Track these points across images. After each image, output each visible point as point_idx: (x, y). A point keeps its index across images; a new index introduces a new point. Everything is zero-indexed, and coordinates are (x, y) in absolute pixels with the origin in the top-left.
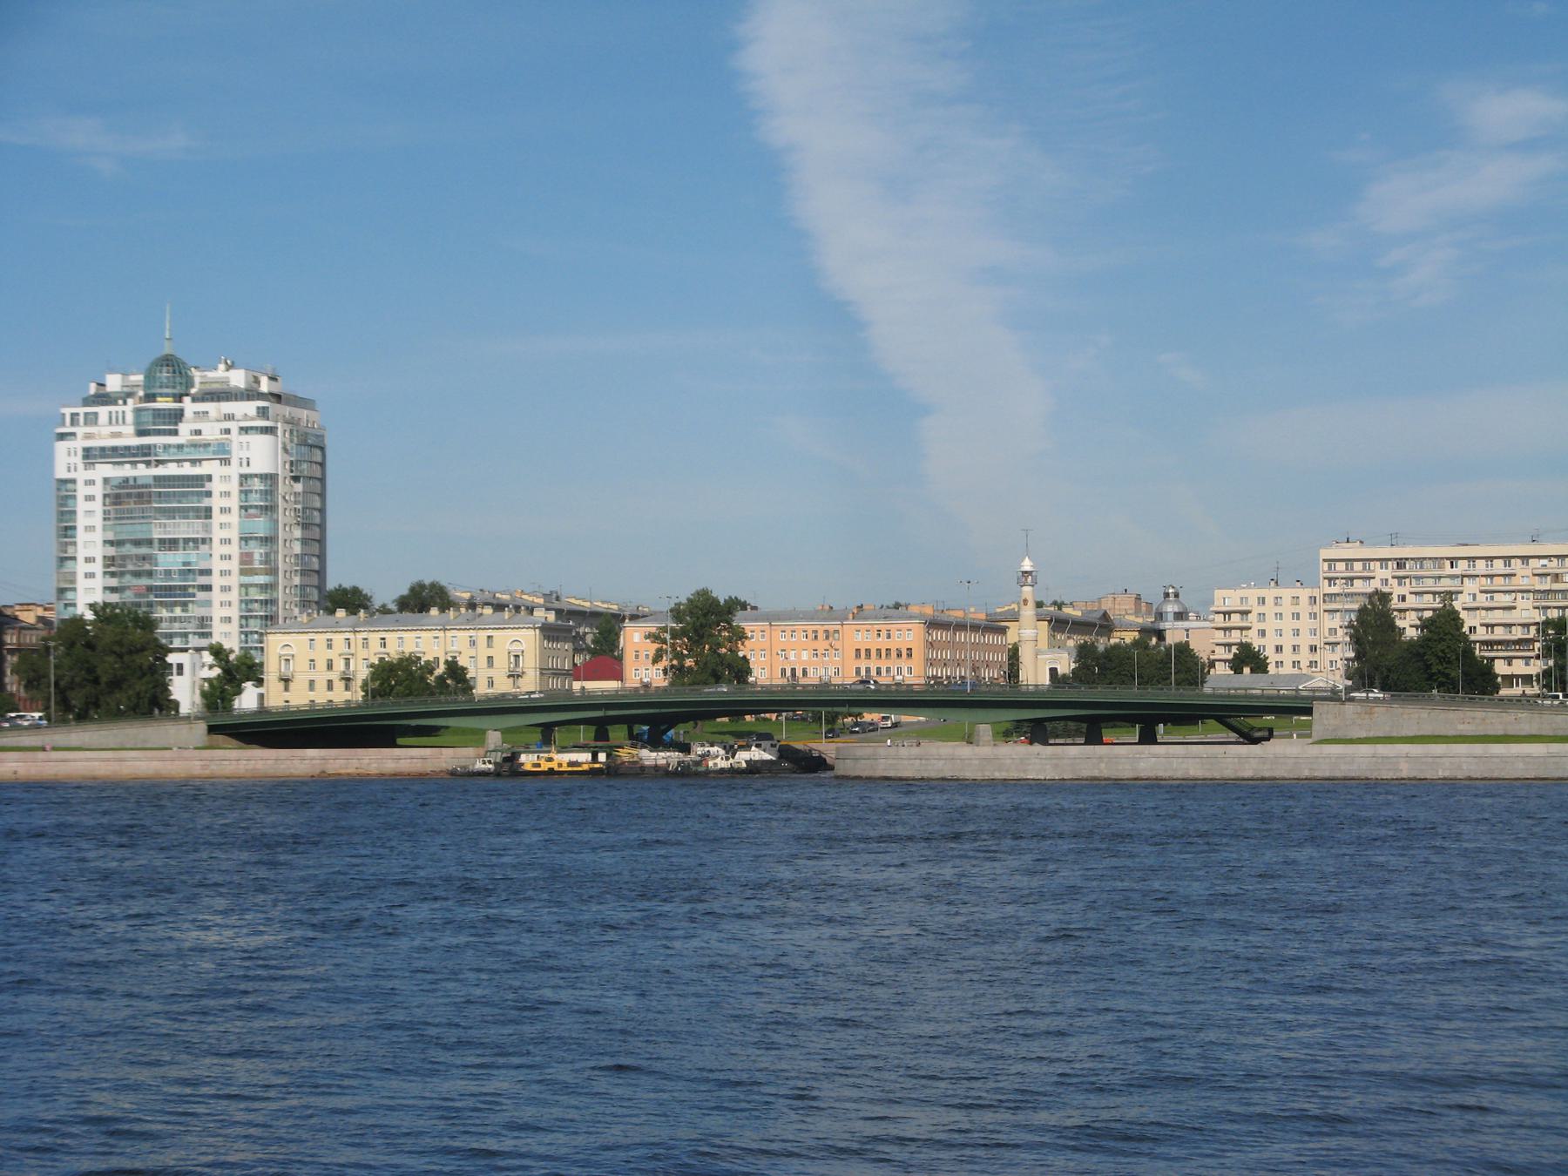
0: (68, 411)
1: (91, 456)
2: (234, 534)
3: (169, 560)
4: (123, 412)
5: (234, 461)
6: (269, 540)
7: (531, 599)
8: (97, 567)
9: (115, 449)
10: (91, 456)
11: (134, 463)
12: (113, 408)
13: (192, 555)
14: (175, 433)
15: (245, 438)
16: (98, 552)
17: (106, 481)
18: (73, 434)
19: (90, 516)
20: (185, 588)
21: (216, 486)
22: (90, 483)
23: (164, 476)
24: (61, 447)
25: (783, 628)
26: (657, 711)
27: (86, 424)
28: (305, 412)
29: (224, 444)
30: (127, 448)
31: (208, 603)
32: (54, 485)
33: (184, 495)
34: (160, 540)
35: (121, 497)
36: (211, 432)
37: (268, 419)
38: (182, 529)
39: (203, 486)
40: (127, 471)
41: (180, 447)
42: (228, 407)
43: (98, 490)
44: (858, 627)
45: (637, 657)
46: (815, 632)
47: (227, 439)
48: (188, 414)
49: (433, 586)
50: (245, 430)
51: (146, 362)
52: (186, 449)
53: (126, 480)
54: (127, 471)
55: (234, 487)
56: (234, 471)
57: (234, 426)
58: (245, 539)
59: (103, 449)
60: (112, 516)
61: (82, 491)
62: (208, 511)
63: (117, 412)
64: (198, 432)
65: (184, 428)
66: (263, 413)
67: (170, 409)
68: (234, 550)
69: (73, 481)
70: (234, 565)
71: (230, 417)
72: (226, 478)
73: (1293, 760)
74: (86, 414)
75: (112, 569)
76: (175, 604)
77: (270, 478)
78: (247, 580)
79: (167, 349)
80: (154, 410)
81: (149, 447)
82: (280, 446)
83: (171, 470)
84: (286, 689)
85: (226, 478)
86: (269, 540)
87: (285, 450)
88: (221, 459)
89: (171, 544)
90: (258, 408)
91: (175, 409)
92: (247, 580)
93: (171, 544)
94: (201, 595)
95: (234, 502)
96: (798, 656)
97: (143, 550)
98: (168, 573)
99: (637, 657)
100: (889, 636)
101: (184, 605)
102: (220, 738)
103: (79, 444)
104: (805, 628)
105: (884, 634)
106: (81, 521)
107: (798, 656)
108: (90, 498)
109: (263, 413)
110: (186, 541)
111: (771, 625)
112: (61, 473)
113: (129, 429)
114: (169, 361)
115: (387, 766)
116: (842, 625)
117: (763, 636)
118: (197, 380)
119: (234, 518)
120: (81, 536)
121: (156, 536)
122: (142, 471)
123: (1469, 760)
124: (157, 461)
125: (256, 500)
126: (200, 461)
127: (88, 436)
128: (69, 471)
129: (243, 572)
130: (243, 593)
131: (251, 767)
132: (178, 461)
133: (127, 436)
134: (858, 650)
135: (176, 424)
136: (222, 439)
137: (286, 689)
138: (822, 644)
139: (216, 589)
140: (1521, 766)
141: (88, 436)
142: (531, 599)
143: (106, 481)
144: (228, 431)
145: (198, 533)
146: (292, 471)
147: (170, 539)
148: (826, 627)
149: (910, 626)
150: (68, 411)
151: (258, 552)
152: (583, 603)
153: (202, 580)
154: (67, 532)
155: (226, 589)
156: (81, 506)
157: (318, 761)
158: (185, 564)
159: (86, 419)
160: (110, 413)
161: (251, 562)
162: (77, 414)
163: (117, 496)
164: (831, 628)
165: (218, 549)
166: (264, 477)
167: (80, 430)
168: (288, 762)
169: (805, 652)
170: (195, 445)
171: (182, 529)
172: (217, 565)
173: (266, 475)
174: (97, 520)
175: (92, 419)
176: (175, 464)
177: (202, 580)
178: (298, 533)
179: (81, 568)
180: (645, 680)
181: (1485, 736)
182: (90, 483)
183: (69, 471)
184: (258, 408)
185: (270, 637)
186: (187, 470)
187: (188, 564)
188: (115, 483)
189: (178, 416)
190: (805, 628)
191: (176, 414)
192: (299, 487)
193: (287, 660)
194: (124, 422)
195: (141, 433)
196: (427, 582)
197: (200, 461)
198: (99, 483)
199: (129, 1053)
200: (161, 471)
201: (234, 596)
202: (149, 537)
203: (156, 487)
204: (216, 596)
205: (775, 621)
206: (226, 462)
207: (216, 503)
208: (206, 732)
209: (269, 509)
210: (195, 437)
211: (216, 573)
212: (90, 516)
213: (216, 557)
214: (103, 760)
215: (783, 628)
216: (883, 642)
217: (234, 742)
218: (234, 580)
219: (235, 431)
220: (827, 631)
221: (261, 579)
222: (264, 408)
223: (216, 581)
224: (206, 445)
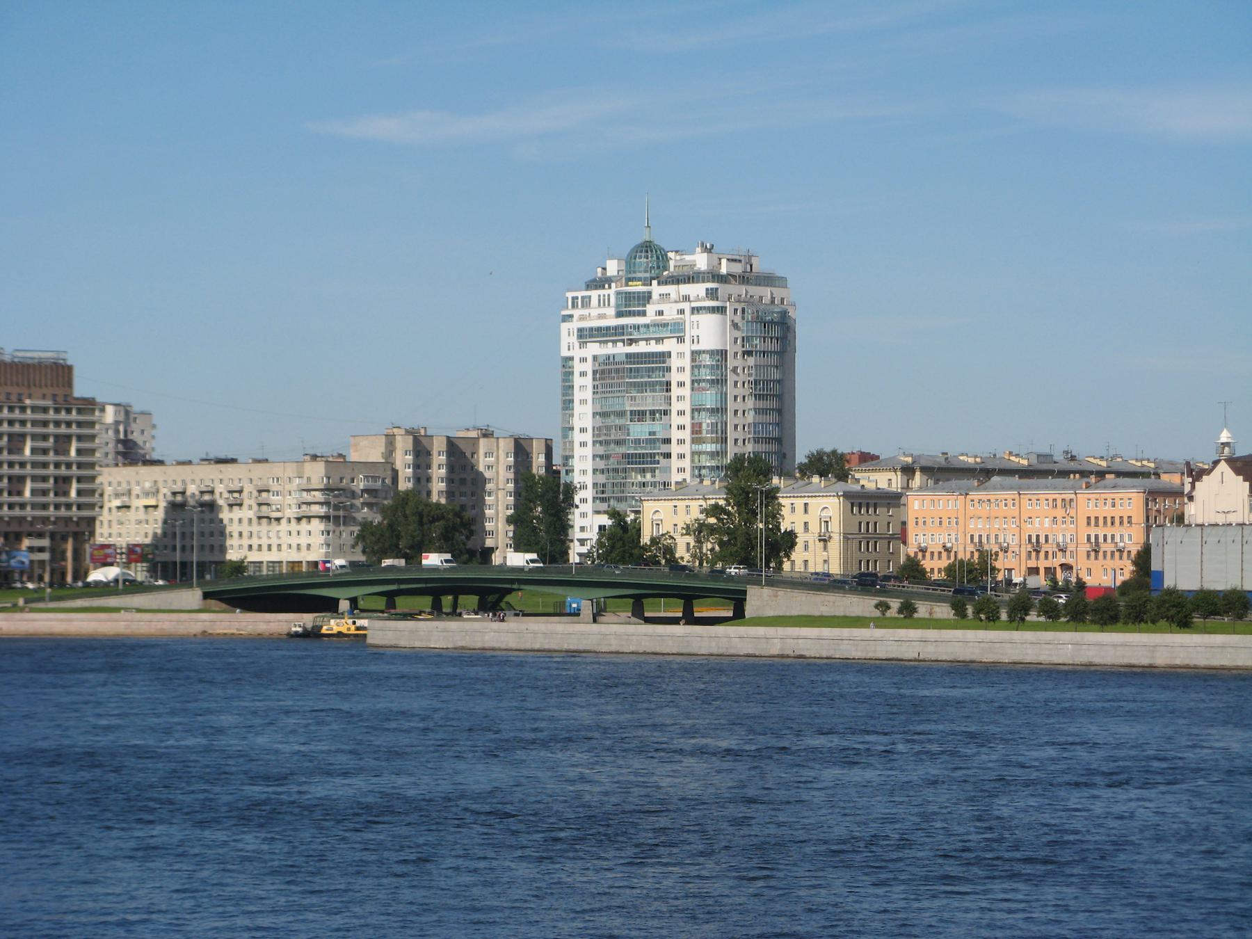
0: (570, 295)
1: (585, 335)
2: (686, 406)
3: (639, 430)
4: (609, 295)
5: (687, 339)
6: (720, 410)
7: (1017, 460)
8: (588, 437)
9: (599, 329)
10: (585, 335)
11: (614, 342)
12: (601, 292)
13: (657, 427)
14: (644, 314)
15: (695, 317)
16: (588, 423)
17: (595, 358)
18: (571, 316)
19: (583, 388)
20: (652, 455)
21: (675, 363)
22: (583, 360)
23: (634, 354)
24: (565, 326)
25: (1029, 497)
26: (424, 586)
27: (583, 306)
28: (769, 289)
29: (679, 323)
30: (608, 328)
31: (668, 470)
32: (560, 364)
33: (653, 370)
34: (631, 411)
35: (605, 372)
36: (670, 313)
37: (717, 300)
38: (649, 401)
39: (664, 362)
40: (609, 349)
41: (647, 326)
42: (685, 289)
43: (588, 367)
44: (1090, 496)
45: (917, 523)
46: (1055, 500)
47: (681, 319)
48: (655, 296)
49: (834, 452)
50: (695, 310)
51: (626, 252)
52: (651, 329)
53: (608, 357)
54: (609, 349)
55: (687, 362)
56: (687, 348)
57: (686, 306)
58: (696, 410)
59: (591, 329)
60: (600, 390)
61: (578, 367)
62: (668, 384)
63: (604, 296)
64: (661, 313)
65: (651, 309)
66: (712, 294)
67: (639, 293)
68: (686, 420)
69: (571, 359)
70: (686, 435)
71: (686, 298)
72: (681, 355)
73: (560, 636)
74: (583, 297)
75: (603, 438)
76: (644, 471)
77: (722, 354)
78: (697, 447)
79: (646, 237)
80: (626, 293)
81: (623, 327)
82: (729, 323)
83: (641, 348)
84: (825, 548)
85: (681, 355)
86: (720, 410)
87: (735, 326)
88: (678, 338)
89: (640, 415)
90: (707, 289)
91: (644, 292)
92: (697, 447)
93: (640, 415)
94: (663, 462)
95: (686, 377)
96: (976, 526)
97: (619, 422)
98: (637, 441)
99: (917, 523)
100: (1114, 506)
101: (653, 471)
102: (212, 603)
103: (575, 325)
104: (1047, 496)
105: (1109, 502)
106: (578, 395)
107: (976, 526)
108: (583, 374)
109: (712, 294)
110: (653, 413)
111: (1020, 494)
112: (565, 353)
113: (611, 311)
114: (647, 247)
115: (261, 627)
116: (1076, 494)
117: (1014, 505)
118: (672, 263)
119: (686, 391)
120: (577, 408)
121: (628, 408)
122: (621, 349)
123: (646, 638)
124: (631, 340)
125: (706, 375)
126: (662, 339)
127: (582, 318)
128: (569, 349)
129: (694, 441)
130: (696, 460)
131: (159, 627)
132: (647, 340)
133: (610, 317)
134: (1089, 518)
135: (644, 305)
136: (677, 319)
137: (825, 548)
138: (1060, 512)
139: (674, 456)
140: (670, 643)
141: (582, 318)
142: (1017, 460)
143: (595, 358)
144: (682, 312)
145: (661, 405)
146: (743, 346)
147: (639, 411)
148: (1063, 496)
149: (1130, 495)
150: (570, 295)
151: (707, 421)
152: (1100, 463)
153: (664, 448)
154: (568, 404)
155: (682, 456)
156: (578, 381)
157: (208, 623)
158: (650, 434)
159: (582, 302)
160: (599, 296)
161: (700, 432)
162: (577, 298)
163: (603, 372)
164: (1068, 497)
165: (676, 420)
166: (712, 353)
167: (577, 313)
168: (187, 623)
169: (1047, 519)
170: (656, 325)
171: (649, 401)
172: (675, 435)
173: (717, 351)
174: (588, 395)
175: (586, 302)
176: (645, 342)
177: (664, 448)
178: (750, 403)
179: (577, 437)
180: (922, 545)
181: (845, 617)
182: (583, 360)
183: (569, 349)
184: (707, 289)
185: (645, 504)
186: (654, 347)
187: (654, 433)
188: (601, 360)
189: (647, 297)
190: (1047, 496)
191: (644, 297)
192: (751, 361)
193: (658, 525)
194: (609, 305)
195: (620, 314)
196: (828, 449)
197: (662, 339)
198: (590, 360)
199: (99, 841)
200: (633, 349)
201: (686, 463)
202: (622, 409)
203: (627, 363)
204: (675, 463)
205: (1024, 489)
206: (681, 340)
207: (675, 377)
208: (201, 598)
209: (720, 382)
210: (680, 316)
211: (674, 442)
212: (583, 388)
213: (674, 427)
214: (58, 620)
215: (1029, 497)
216: (1107, 511)
217: (224, 606)
218: (686, 449)
219: (688, 312)
220: (1063, 500)
221: (710, 447)
222: (712, 289)
223: (675, 449)
224: (665, 325)
